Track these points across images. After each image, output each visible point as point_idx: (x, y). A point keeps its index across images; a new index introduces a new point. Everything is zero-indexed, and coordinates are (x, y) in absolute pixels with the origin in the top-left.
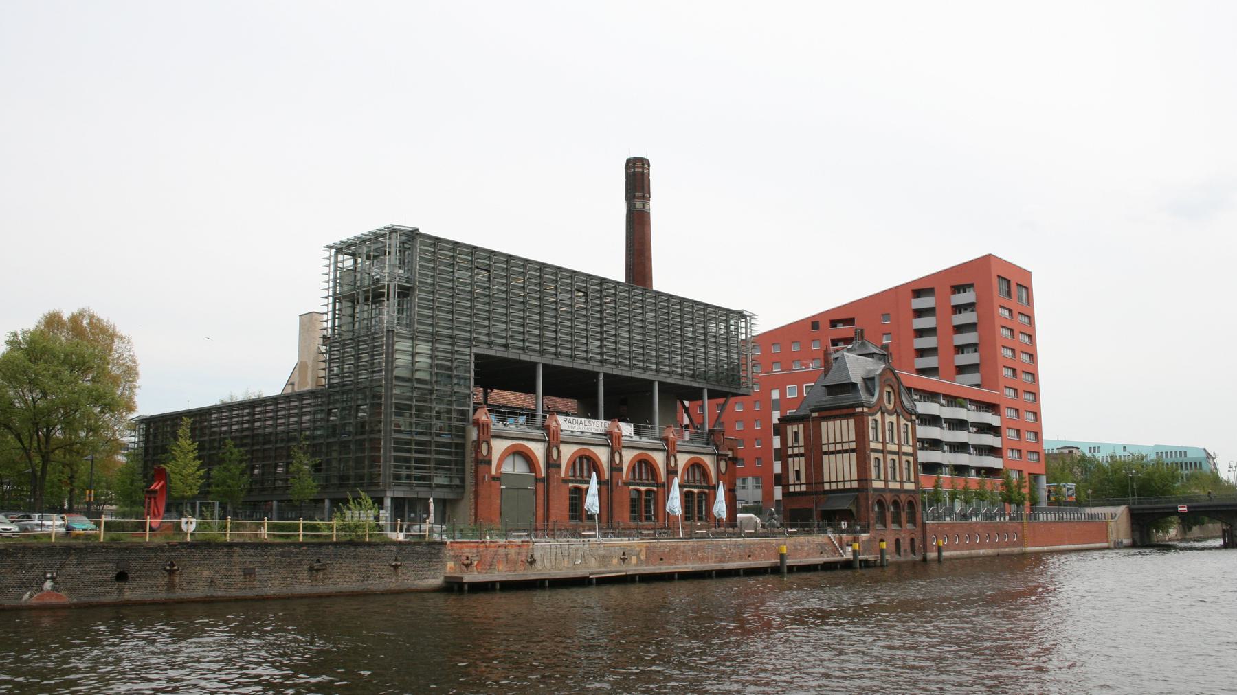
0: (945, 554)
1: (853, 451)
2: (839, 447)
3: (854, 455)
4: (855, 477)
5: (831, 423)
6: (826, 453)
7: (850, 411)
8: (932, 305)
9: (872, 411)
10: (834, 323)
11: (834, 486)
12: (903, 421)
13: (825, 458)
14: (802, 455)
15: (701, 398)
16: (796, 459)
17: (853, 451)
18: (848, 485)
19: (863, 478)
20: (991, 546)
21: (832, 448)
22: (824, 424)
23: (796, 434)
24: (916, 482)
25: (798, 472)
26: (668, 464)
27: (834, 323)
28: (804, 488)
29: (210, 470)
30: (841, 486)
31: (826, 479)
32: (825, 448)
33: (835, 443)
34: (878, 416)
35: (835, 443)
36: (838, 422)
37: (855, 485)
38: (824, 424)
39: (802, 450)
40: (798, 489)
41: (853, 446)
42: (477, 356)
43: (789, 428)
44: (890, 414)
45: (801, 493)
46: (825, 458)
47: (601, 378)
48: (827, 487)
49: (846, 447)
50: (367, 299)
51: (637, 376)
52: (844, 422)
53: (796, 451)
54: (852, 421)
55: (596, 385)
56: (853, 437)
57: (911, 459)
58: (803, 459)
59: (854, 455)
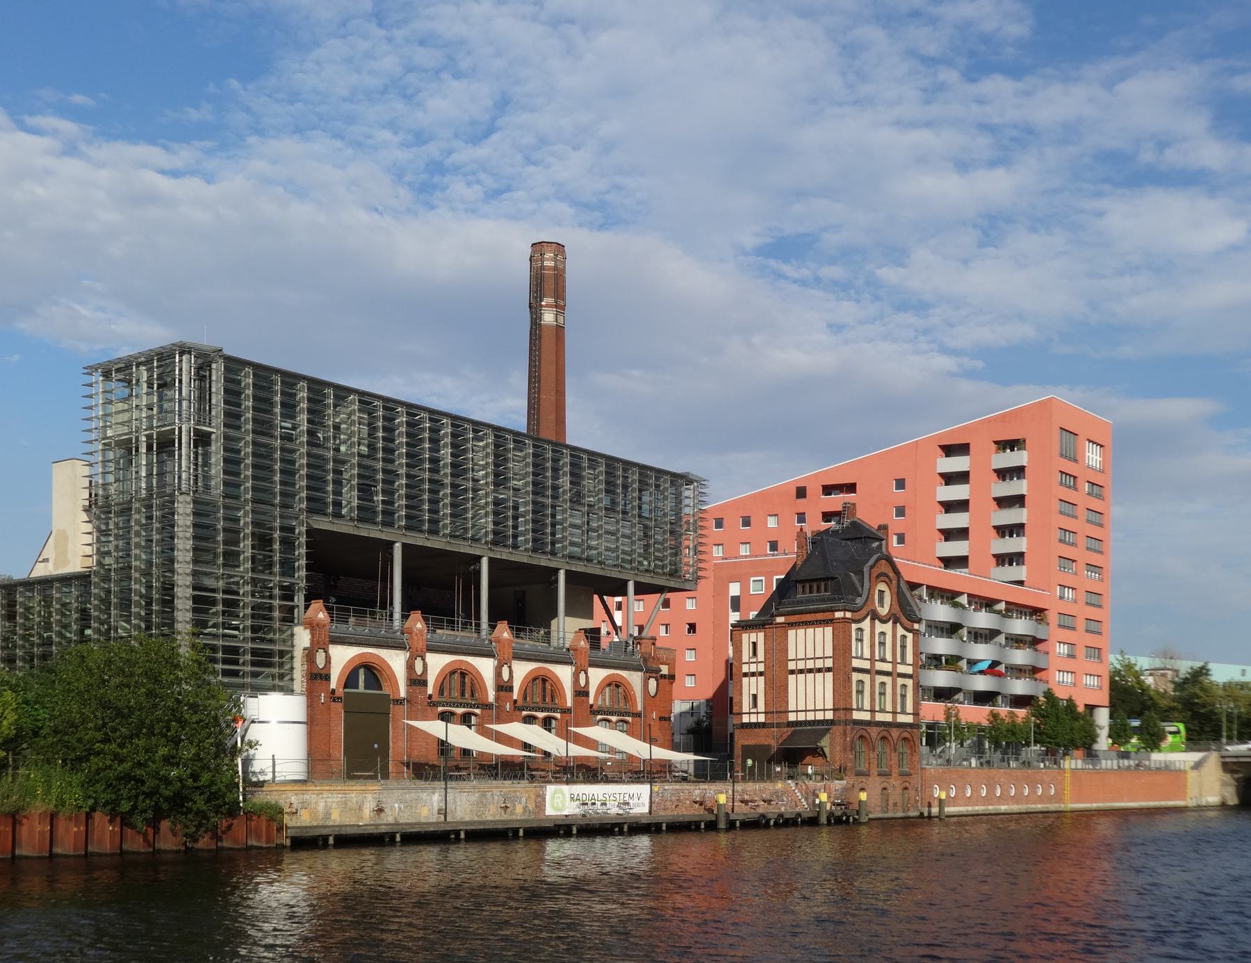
0: (949, 810)
1: (829, 670)
2: (810, 665)
4: (830, 705)
5: (801, 632)
6: (792, 672)
7: (828, 616)
9: (858, 616)
10: (828, 490)
11: (801, 717)
12: (900, 631)
13: (792, 678)
14: (761, 674)
16: (753, 679)
17: (829, 670)
18: (820, 716)
19: (842, 706)
21: (801, 665)
22: (791, 633)
25: (755, 697)
26: (498, 674)
28: (762, 718)
30: (810, 717)
31: (792, 707)
32: (792, 666)
33: (806, 659)
36: (810, 631)
37: (829, 715)
38: (791, 633)
39: (761, 668)
40: (753, 719)
43: (745, 636)
49: (819, 664)
51: (420, 543)
52: (819, 630)
53: (753, 668)
54: (829, 630)
56: (829, 652)
57: (909, 682)
58: (762, 679)
59: (829, 676)
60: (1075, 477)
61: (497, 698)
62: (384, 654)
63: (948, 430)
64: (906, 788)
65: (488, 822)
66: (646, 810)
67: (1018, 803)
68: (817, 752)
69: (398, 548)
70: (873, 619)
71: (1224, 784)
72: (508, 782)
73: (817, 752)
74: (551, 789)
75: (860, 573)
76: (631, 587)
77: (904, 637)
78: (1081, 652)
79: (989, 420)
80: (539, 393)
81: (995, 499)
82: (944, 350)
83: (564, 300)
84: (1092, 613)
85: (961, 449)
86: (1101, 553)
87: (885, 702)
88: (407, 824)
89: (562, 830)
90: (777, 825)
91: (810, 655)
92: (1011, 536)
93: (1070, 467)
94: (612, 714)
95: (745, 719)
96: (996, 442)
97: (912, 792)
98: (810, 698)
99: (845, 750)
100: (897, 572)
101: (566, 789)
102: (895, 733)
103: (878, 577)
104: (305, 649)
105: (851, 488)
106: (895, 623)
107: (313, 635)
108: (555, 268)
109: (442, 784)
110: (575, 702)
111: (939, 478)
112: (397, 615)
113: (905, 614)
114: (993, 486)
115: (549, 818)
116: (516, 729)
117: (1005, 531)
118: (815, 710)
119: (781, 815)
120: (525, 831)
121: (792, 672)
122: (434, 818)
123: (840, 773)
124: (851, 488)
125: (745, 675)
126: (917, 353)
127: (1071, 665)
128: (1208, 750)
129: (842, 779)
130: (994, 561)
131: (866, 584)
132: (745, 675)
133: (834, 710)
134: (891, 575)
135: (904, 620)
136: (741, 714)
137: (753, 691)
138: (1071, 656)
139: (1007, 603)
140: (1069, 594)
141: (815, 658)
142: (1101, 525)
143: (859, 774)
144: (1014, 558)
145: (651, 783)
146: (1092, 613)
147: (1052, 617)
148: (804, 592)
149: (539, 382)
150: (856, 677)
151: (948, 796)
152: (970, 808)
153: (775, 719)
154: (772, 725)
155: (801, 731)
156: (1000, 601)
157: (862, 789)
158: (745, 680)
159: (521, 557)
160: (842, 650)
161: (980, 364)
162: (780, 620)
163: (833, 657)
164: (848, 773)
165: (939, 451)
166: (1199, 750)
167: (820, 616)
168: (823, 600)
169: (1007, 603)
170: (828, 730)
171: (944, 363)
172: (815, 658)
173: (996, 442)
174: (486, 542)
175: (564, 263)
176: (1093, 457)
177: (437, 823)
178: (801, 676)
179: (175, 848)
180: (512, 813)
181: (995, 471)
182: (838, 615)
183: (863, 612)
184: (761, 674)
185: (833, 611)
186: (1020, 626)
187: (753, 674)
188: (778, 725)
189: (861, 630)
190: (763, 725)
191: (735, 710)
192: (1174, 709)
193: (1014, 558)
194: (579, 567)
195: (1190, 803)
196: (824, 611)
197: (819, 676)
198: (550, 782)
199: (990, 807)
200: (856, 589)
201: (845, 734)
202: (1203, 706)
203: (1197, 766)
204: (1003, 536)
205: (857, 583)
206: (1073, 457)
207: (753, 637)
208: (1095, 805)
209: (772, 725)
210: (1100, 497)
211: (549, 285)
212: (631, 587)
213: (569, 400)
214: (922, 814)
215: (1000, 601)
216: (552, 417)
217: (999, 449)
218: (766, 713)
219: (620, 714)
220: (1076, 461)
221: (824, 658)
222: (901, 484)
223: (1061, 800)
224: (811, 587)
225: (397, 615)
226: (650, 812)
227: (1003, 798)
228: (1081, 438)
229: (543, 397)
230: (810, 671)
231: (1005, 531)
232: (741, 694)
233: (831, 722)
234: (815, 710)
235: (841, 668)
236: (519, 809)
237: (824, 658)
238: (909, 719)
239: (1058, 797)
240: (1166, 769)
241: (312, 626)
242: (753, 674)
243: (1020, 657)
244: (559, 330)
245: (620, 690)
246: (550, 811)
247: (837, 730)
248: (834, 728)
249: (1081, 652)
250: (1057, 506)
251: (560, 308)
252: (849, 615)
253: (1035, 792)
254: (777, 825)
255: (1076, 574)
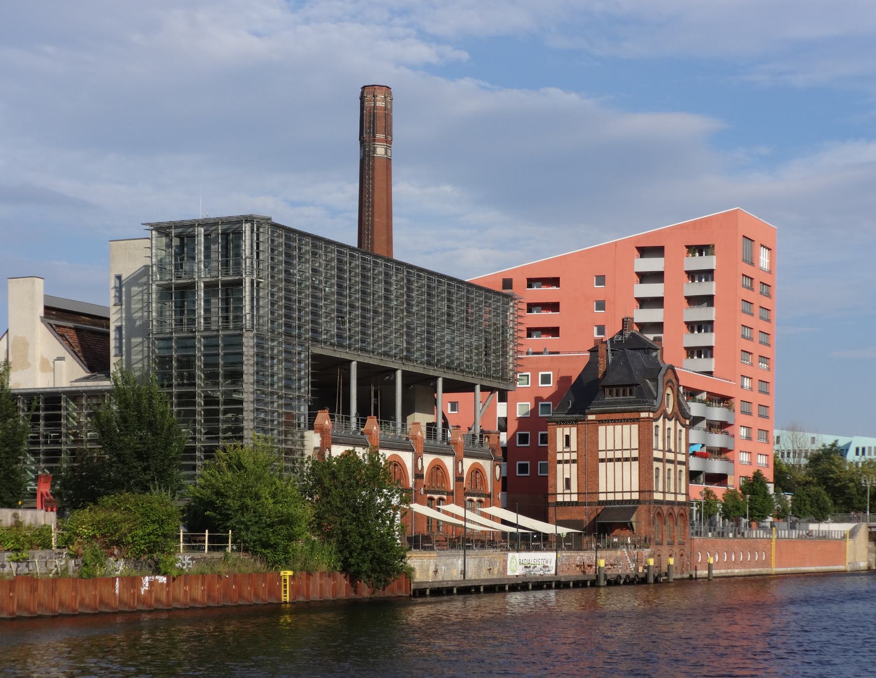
0: (715, 572)
1: (635, 459)
2: (618, 455)
3: (635, 464)
4: (636, 487)
5: (610, 428)
6: (602, 460)
7: (634, 415)
8: (660, 268)
10: (531, 282)
11: (611, 497)
12: (679, 427)
13: (602, 466)
14: (574, 461)
15: (473, 390)
16: (567, 466)
17: (635, 459)
18: (627, 497)
19: (646, 489)
20: (743, 564)
21: (610, 455)
22: (601, 429)
23: (568, 438)
24: (687, 494)
25: (568, 482)
26: (416, 465)
27: (531, 282)
28: (575, 498)
29: (585, 534)
30: (619, 497)
31: (602, 488)
32: (602, 455)
33: (614, 450)
34: (660, 422)
35: (614, 450)
36: (618, 427)
37: (636, 496)
38: (601, 429)
39: (574, 456)
40: (567, 498)
41: (635, 454)
42: (315, 357)
43: (559, 430)
44: (670, 420)
45: (571, 504)
46: (602, 466)
47: (399, 374)
48: (602, 497)
49: (627, 454)
50: (789, 453)
51: (421, 371)
52: (626, 427)
53: (567, 457)
54: (635, 427)
55: (393, 383)
56: (635, 445)
57: (683, 468)
58: (574, 466)
59: (635, 464)
60: (752, 279)
61: (415, 484)
62: (401, 454)
63: (645, 233)
64: (682, 555)
65: (495, 579)
66: (553, 572)
67: (745, 567)
68: (628, 526)
69: (354, 365)
70: (664, 418)
71: (870, 551)
72: (491, 550)
73: (628, 526)
74: (511, 555)
75: (655, 380)
76: (478, 388)
77: (680, 431)
78: (755, 434)
79: (681, 227)
80: (373, 216)
81: (686, 297)
82: (424, 37)
83: (391, 136)
84: (763, 399)
85: (658, 251)
86: (769, 345)
87: (672, 488)
88: (475, 580)
89: (520, 586)
90: (625, 583)
91: (618, 447)
92: (699, 331)
93: (749, 270)
94: (474, 495)
95: (560, 498)
96: (687, 247)
97: (685, 558)
98: (618, 482)
99: (649, 524)
100: (677, 379)
101: (517, 555)
102: (665, 508)
103: (667, 382)
104: (316, 448)
105: (555, 281)
106: (676, 420)
107: (323, 438)
108: (386, 108)
109: (462, 552)
110: (456, 486)
111: (635, 275)
112: (354, 420)
113: (681, 414)
114: (685, 285)
115: (509, 579)
116: (452, 508)
117: (695, 326)
118: (623, 492)
119: (628, 576)
120: (431, 591)
121: (602, 460)
122: (459, 577)
123: (646, 542)
124: (555, 281)
125: (560, 462)
126: (392, 38)
127: (749, 446)
128: (858, 520)
129: (648, 548)
130: (685, 352)
131: (660, 390)
132: (560, 462)
133: (639, 492)
134: (674, 380)
135: (681, 418)
136: (556, 494)
137: (567, 476)
138: (749, 438)
139: (708, 393)
140: (747, 383)
141: (622, 450)
142: (769, 321)
143: (657, 544)
144: (705, 351)
145: (556, 551)
146: (763, 399)
147: (737, 404)
148: (617, 395)
149: (373, 206)
150: (656, 464)
151: (714, 561)
152: (757, 570)
153: (588, 498)
154: (584, 504)
155: (609, 509)
156: (701, 391)
157: (671, 556)
158: (559, 466)
159: (327, 351)
160: (646, 443)
161: (465, 55)
162: (591, 417)
163: (639, 449)
164: (652, 542)
165: (636, 252)
166: (850, 520)
167: (627, 416)
168: (630, 403)
169: (708, 393)
170: (635, 509)
171: (422, 52)
172: (622, 450)
173: (687, 247)
174: (421, 363)
175: (391, 103)
176: (764, 259)
177: (459, 581)
178: (610, 464)
179: (9, 617)
180: (493, 574)
181: (687, 272)
182: (643, 415)
183: (659, 412)
184: (574, 461)
185: (639, 411)
186: (717, 413)
187: (567, 462)
188: (590, 504)
189: (657, 427)
190: (576, 504)
191: (550, 490)
192: (810, 483)
193: (705, 351)
194: (450, 376)
195: (847, 567)
196: (631, 411)
197: (627, 464)
198: (509, 551)
199: (729, 571)
200: (651, 393)
201: (649, 511)
202: (837, 480)
203: (853, 533)
204: (692, 331)
205: (652, 388)
206: (751, 261)
207: (567, 431)
208: (789, 569)
209: (584, 504)
210: (769, 296)
211: (380, 124)
212: (478, 388)
213: (395, 221)
214: (691, 576)
215: (701, 391)
216: (384, 238)
217: (689, 252)
218: (578, 493)
219: (479, 495)
220: (752, 264)
221: (631, 449)
222: (601, 280)
223: (769, 566)
224: (624, 391)
225: (354, 420)
226: (556, 574)
227: (736, 564)
228: (757, 244)
229: (376, 220)
230: (619, 460)
231: (695, 326)
232: (556, 478)
233: (637, 502)
234: (623, 492)
235: (644, 458)
236: (496, 571)
237: (631, 449)
238: (682, 498)
239: (767, 563)
240: (824, 537)
241: (322, 431)
242: (567, 462)
243: (717, 440)
244: (388, 161)
245: (478, 476)
246: (510, 573)
247: (642, 508)
248: (640, 507)
249: (755, 434)
250: (740, 305)
251: (388, 142)
252: (651, 415)
253: (754, 558)
254: (625, 583)
255: (752, 365)
